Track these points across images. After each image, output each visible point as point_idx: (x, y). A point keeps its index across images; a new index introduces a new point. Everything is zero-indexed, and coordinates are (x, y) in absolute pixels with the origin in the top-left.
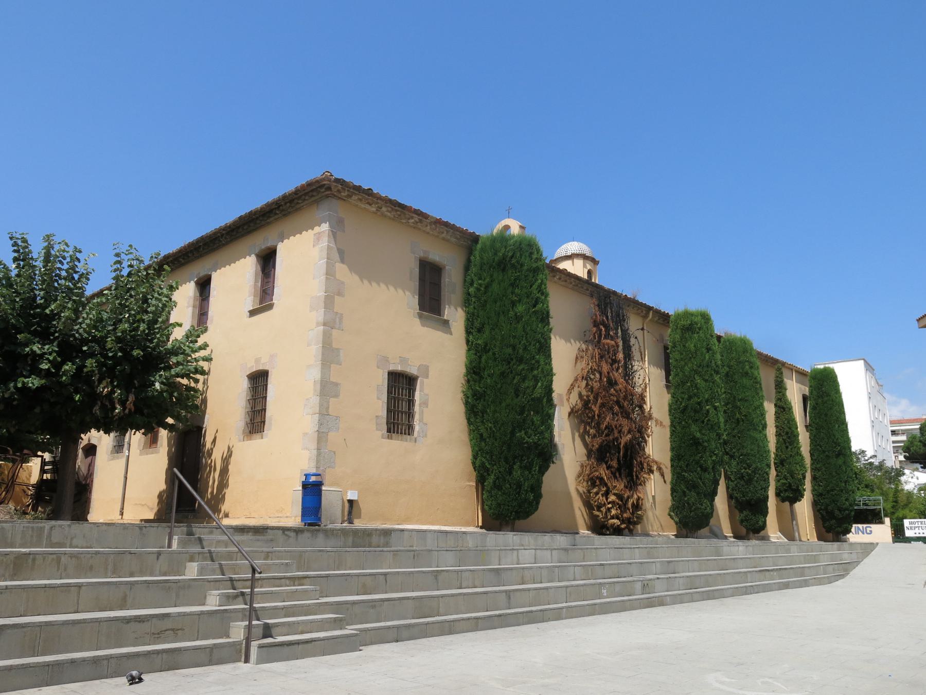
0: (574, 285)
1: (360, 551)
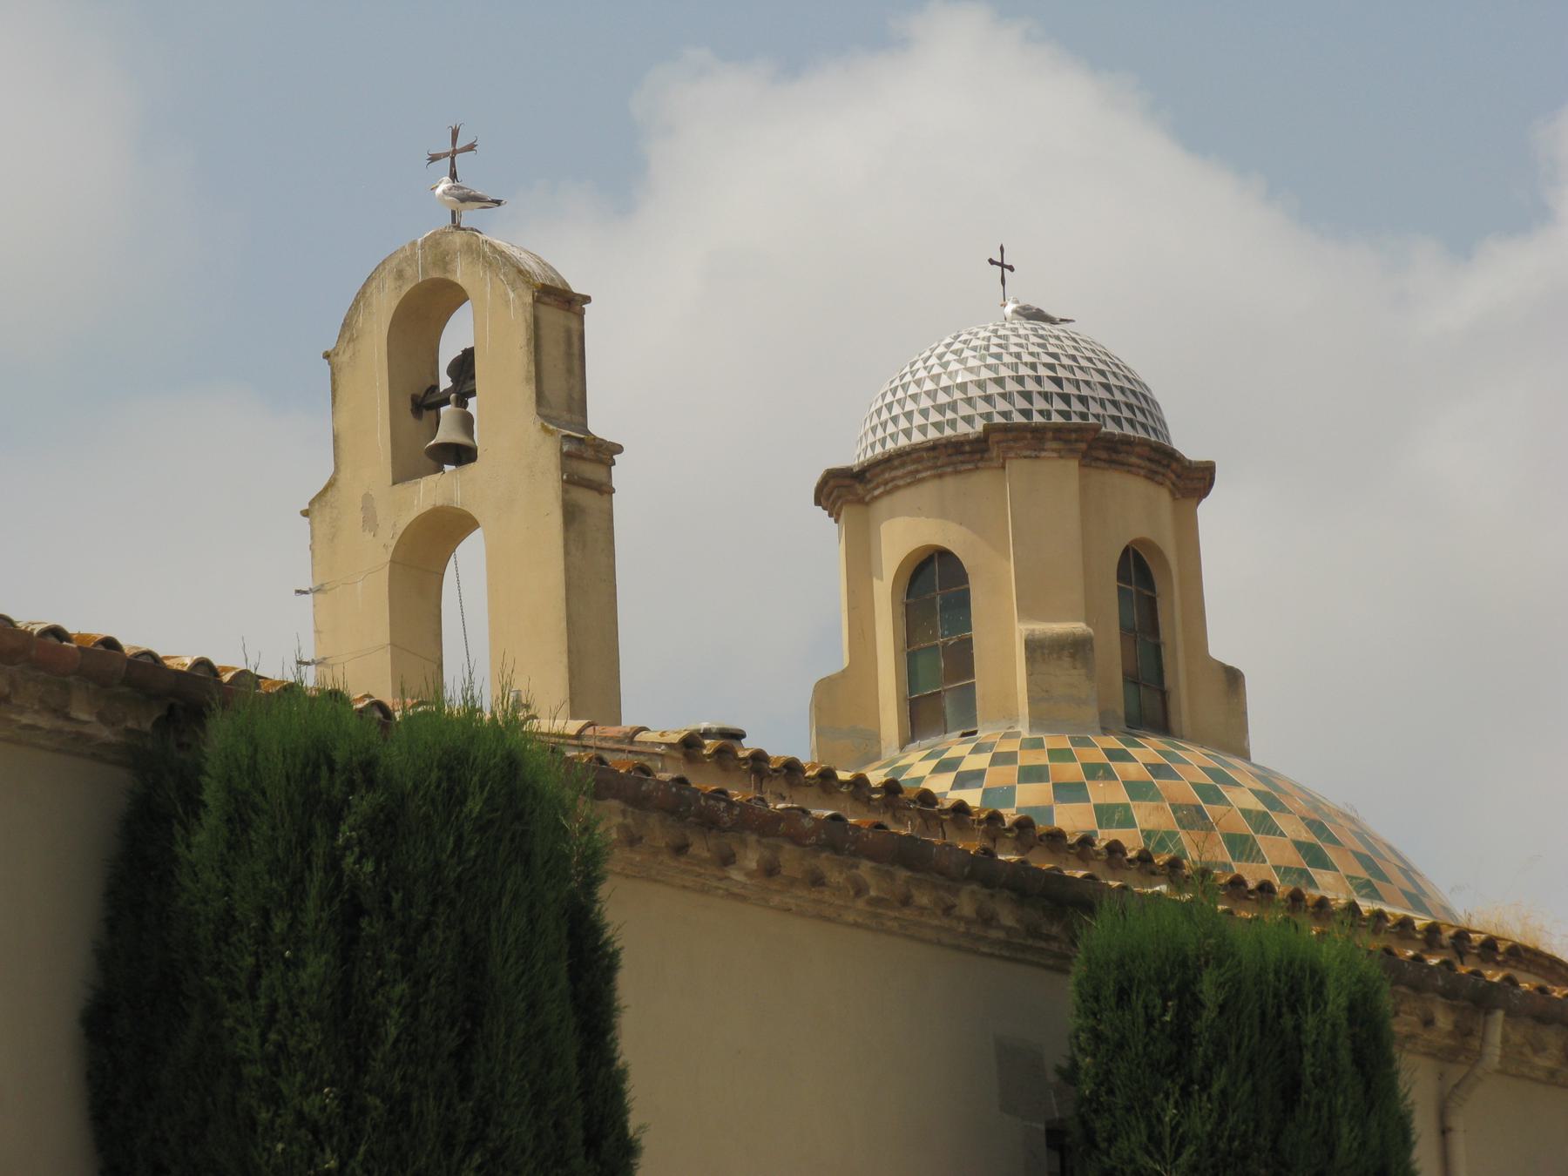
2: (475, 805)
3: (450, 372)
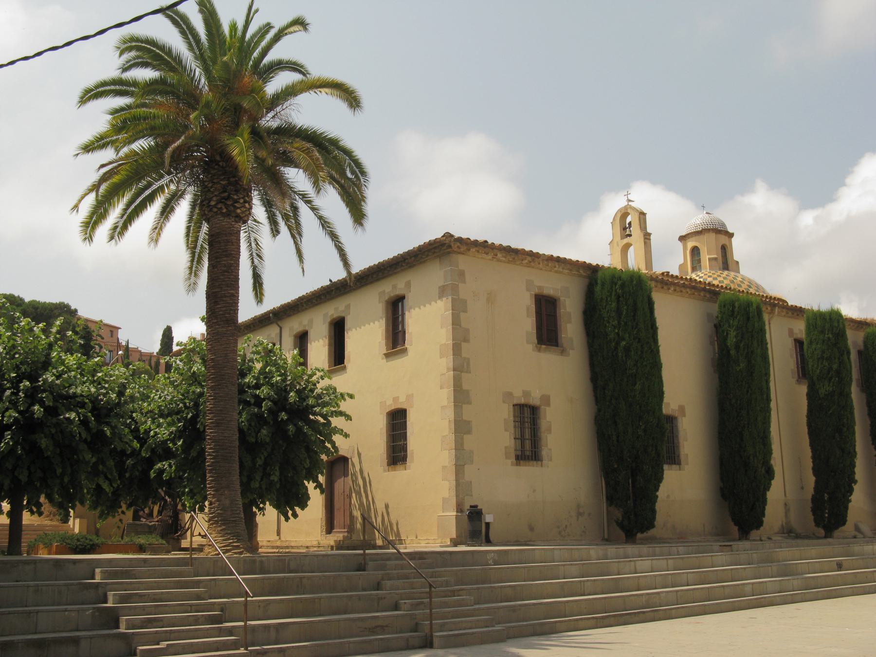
0: (689, 294)
1: (417, 593)
2: (635, 282)
3: (628, 224)
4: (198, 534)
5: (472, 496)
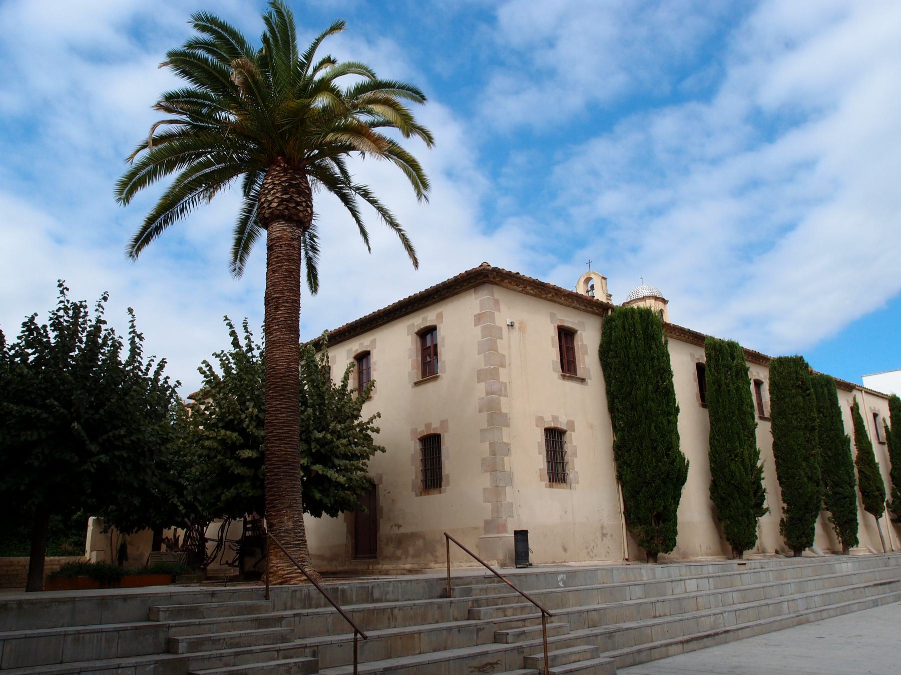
4: (225, 562)
5: (513, 517)
